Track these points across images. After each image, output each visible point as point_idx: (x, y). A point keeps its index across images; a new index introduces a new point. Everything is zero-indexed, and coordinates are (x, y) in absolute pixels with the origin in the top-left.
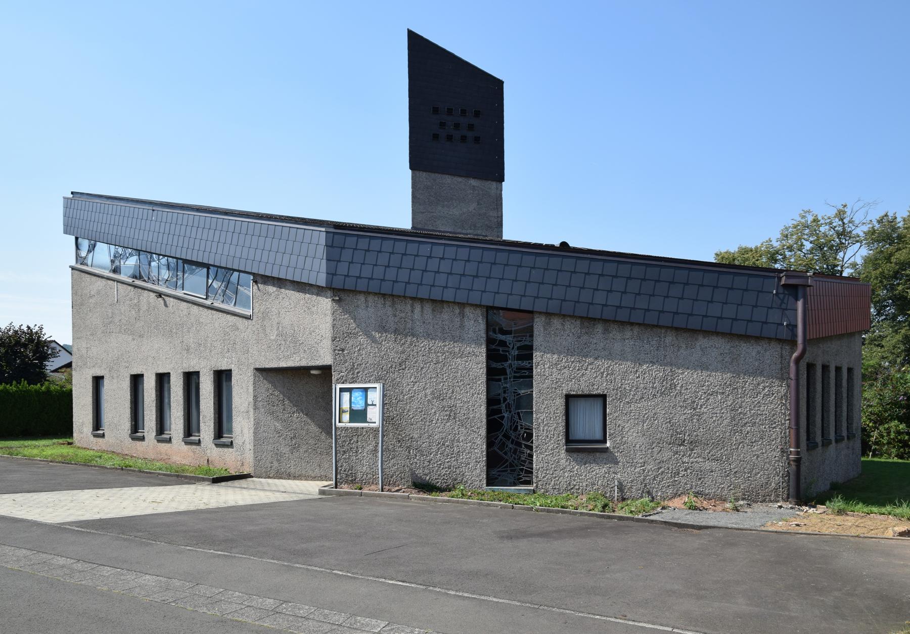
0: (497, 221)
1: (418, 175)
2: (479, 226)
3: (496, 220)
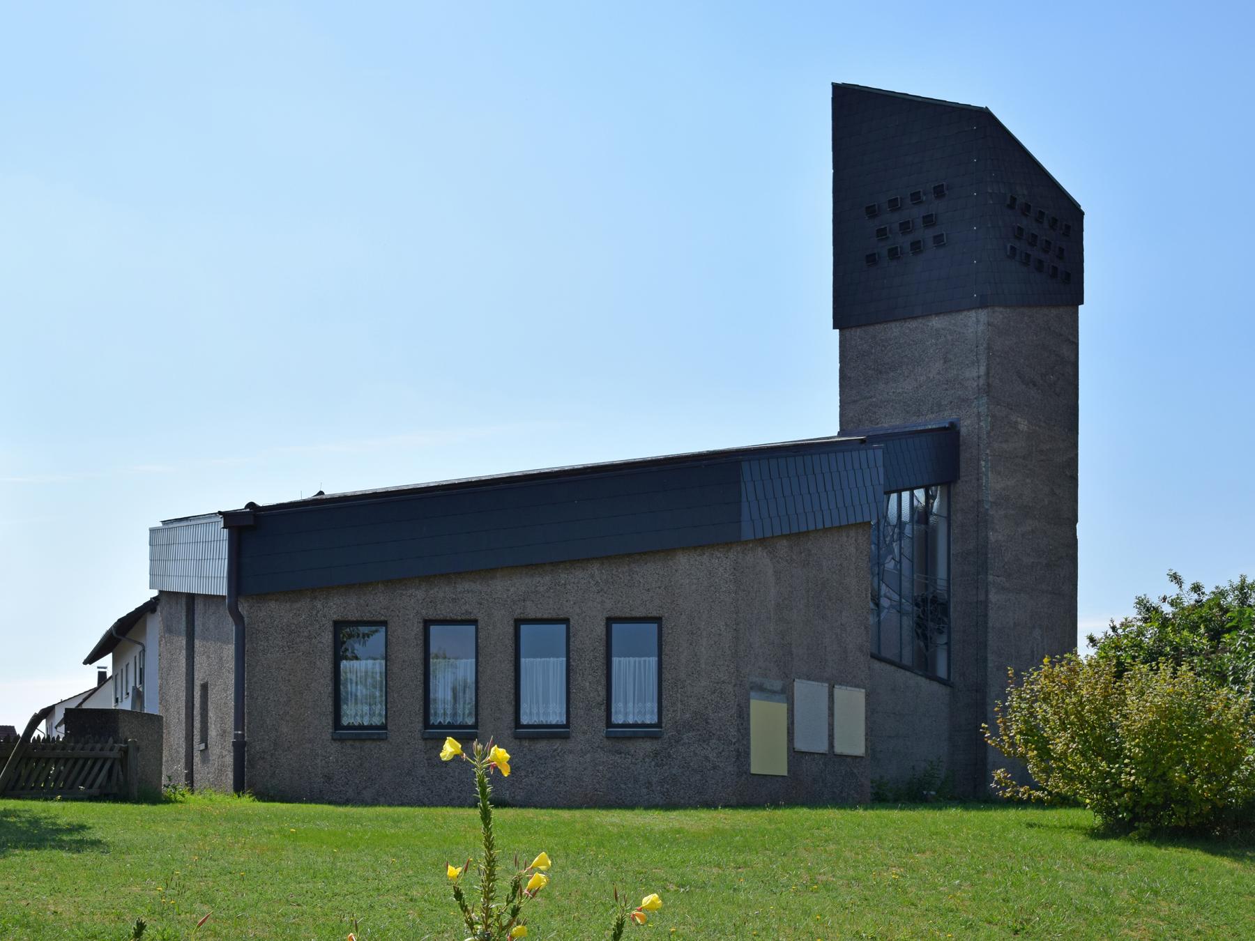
0: (978, 385)
1: (963, 474)
2: (946, 403)
3: (976, 384)
